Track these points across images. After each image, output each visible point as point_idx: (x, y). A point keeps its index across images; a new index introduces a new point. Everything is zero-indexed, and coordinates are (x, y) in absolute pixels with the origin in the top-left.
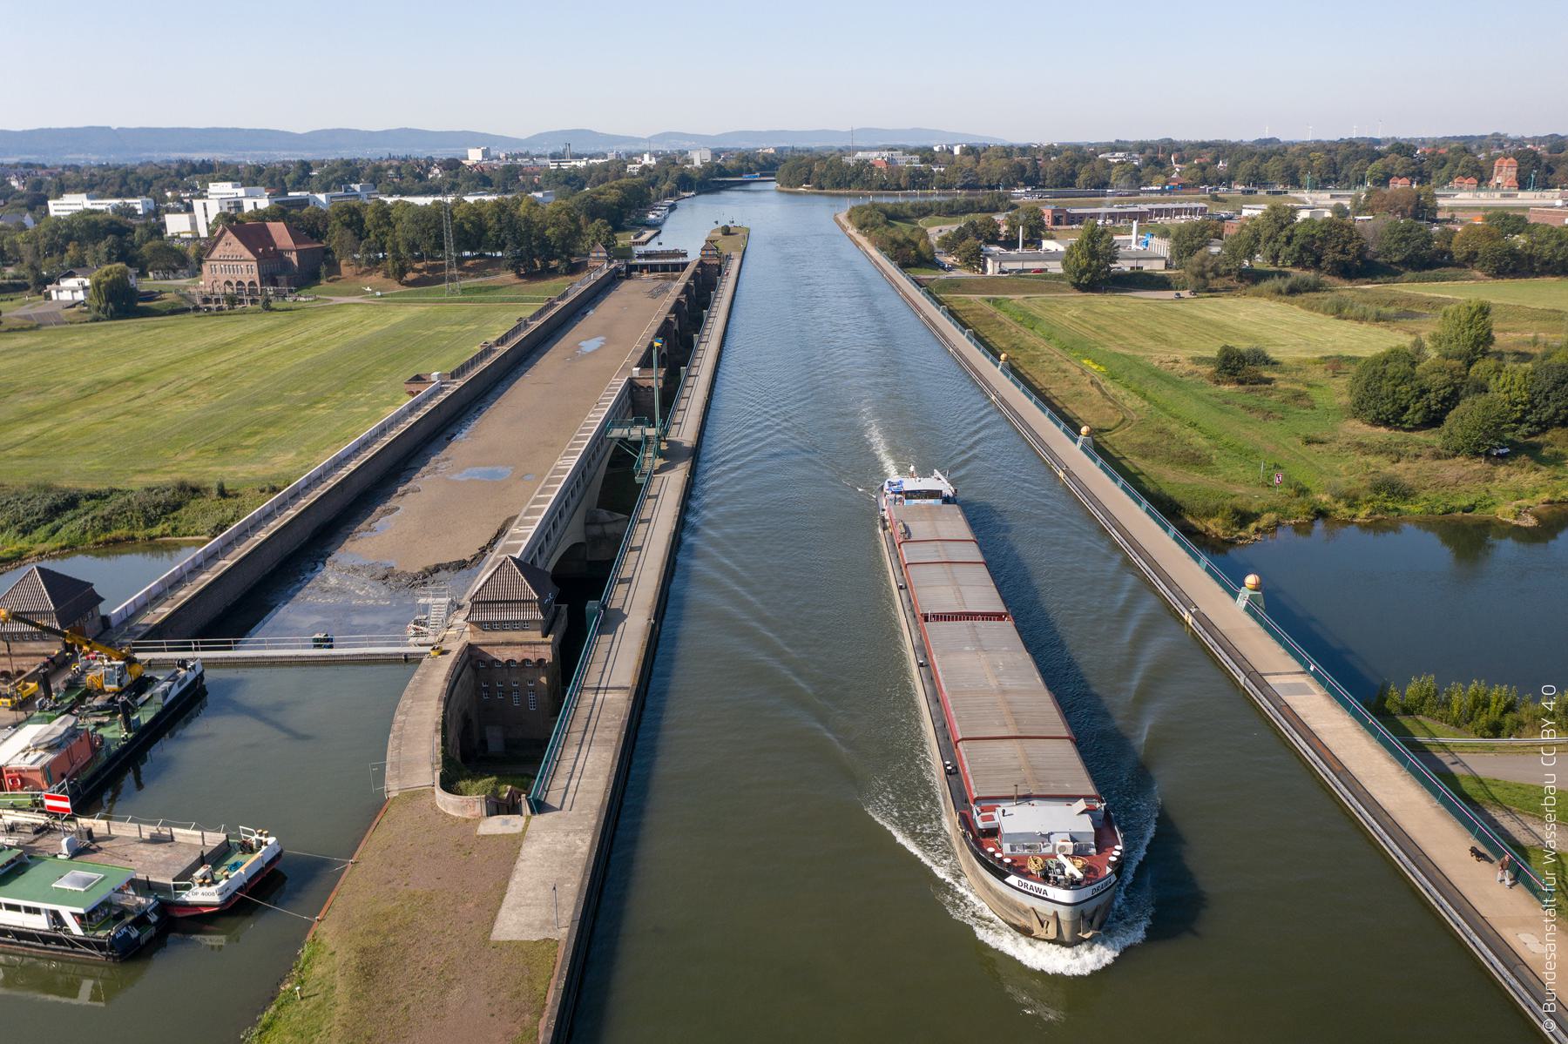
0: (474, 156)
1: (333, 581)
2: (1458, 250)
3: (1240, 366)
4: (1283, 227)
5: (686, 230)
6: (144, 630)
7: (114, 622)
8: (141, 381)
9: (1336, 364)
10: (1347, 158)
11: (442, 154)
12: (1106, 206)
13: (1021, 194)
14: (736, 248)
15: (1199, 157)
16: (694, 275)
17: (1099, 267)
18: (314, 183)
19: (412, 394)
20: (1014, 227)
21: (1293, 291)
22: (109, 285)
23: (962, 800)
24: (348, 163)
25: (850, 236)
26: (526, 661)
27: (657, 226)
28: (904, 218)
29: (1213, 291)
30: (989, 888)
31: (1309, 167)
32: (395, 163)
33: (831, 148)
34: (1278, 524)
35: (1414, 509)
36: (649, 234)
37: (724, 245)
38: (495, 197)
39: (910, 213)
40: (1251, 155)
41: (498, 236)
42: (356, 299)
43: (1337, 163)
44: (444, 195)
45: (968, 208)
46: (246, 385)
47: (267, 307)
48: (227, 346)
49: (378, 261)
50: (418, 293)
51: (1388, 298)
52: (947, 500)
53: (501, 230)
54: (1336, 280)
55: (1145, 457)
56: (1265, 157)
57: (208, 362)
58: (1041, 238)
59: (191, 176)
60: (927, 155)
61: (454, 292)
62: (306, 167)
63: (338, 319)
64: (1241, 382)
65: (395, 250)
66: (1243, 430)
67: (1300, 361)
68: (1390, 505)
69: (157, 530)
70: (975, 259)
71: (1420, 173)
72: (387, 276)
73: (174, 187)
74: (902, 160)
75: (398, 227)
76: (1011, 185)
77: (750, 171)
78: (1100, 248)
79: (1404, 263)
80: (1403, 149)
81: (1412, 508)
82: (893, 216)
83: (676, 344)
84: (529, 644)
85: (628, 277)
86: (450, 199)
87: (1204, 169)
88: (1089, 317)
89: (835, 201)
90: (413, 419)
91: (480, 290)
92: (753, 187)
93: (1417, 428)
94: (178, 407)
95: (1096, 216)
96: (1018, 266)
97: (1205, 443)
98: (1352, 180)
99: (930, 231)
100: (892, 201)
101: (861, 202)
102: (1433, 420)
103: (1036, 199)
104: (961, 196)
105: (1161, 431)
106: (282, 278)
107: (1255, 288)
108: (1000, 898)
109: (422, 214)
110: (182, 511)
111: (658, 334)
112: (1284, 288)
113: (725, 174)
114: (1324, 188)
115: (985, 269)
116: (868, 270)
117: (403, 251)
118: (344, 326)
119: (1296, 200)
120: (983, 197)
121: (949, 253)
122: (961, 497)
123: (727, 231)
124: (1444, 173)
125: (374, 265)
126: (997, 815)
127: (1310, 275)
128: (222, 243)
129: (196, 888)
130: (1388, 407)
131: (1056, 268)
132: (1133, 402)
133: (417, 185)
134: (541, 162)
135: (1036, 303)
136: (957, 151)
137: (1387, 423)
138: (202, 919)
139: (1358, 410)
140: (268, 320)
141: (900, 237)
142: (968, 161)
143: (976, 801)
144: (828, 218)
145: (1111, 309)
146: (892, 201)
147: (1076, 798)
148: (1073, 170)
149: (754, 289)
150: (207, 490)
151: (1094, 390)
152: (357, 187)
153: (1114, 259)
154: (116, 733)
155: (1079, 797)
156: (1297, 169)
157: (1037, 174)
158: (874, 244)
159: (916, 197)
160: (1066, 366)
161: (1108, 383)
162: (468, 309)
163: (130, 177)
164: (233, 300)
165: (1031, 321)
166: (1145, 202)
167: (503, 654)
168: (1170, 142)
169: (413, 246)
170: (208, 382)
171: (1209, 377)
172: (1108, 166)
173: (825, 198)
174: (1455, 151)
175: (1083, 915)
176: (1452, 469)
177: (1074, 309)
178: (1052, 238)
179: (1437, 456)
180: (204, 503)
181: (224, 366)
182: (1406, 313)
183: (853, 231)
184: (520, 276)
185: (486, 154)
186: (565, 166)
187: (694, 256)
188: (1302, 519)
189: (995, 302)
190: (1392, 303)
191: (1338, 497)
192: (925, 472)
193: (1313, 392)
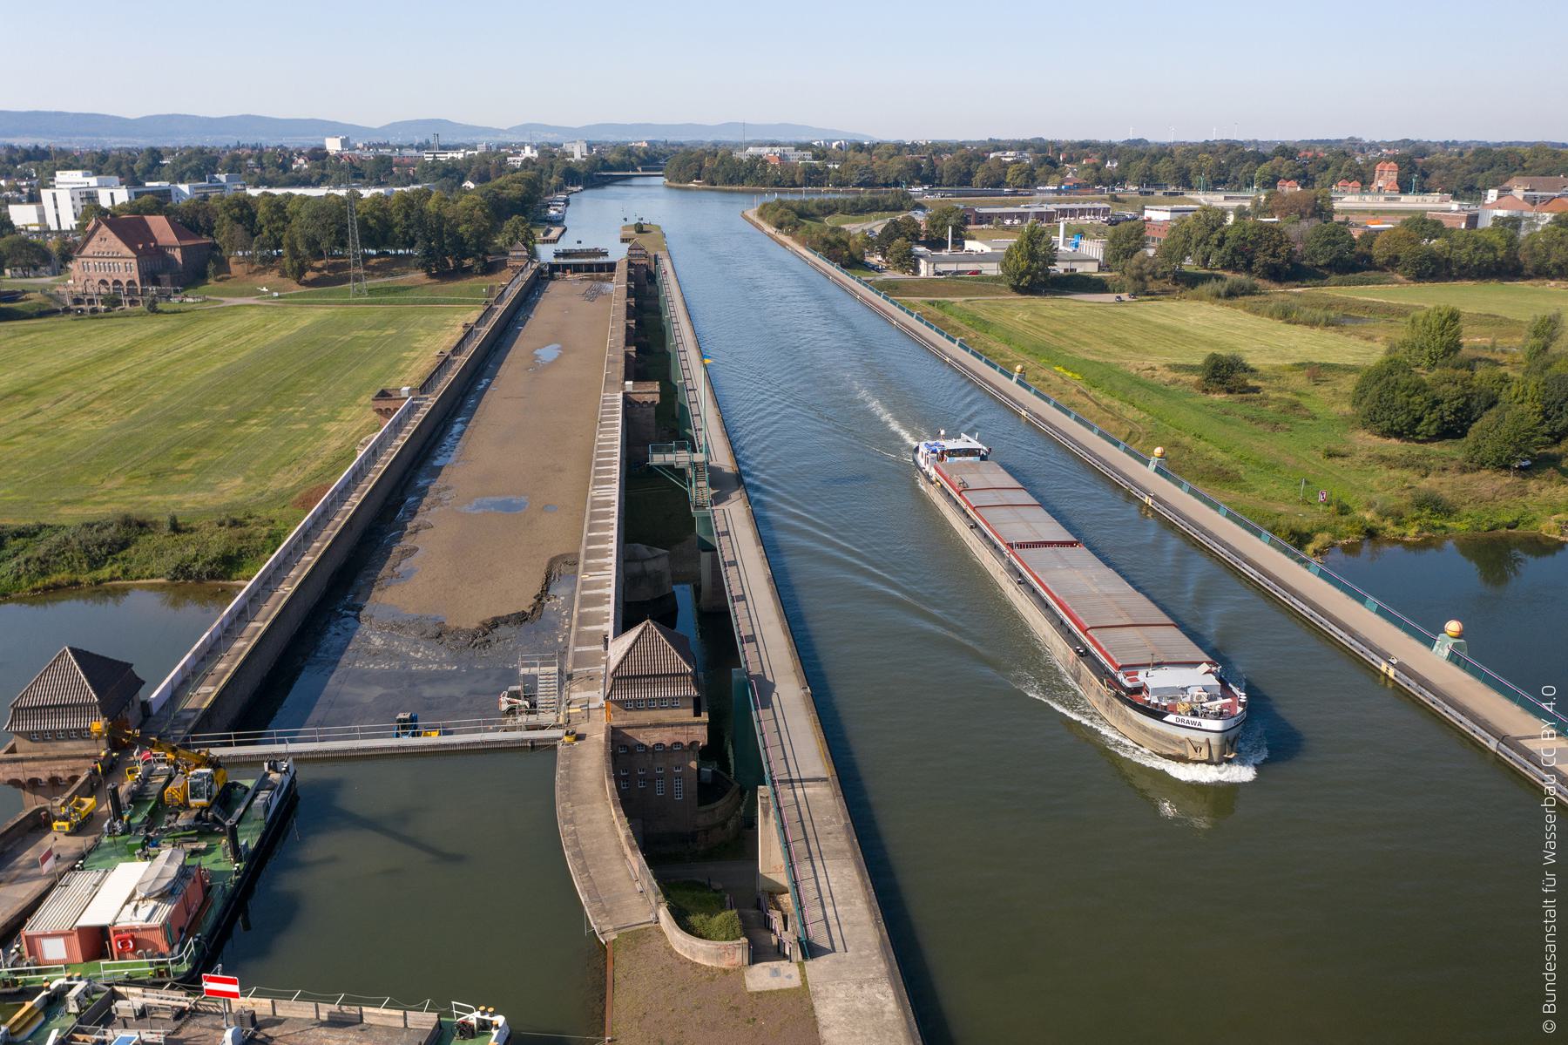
1: (377, 642)
2: (1378, 252)
3: (1224, 373)
4: (1214, 229)
6: (194, 719)
7: (155, 709)
11: (308, 142)
15: (1087, 157)
18: (167, 172)
21: (1231, 294)
24: (201, 151)
25: (769, 235)
27: (558, 222)
35: (1460, 526)
36: (555, 232)
38: (374, 191)
39: (815, 211)
41: (406, 233)
43: (1229, 164)
44: (337, 186)
46: (158, 398)
47: (153, 309)
49: (273, 259)
50: (320, 294)
54: (1267, 283)
57: (105, 371)
60: (822, 154)
61: (359, 293)
62: (155, 154)
63: (238, 323)
64: (1230, 391)
66: (1255, 443)
67: (1274, 368)
68: (1437, 523)
69: (105, 572)
70: (909, 262)
71: (1305, 175)
72: (283, 274)
74: (794, 157)
79: (1328, 266)
81: (1458, 525)
82: (803, 214)
83: (648, 350)
84: (682, 725)
85: (552, 278)
86: (342, 192)
88: (1040, 321)
89: (727, 198)
90: (400, 443)
91: (388, 291)
92: (636, 181)
93: (1431, 439)
96: (953, 267)
98: (1242, 180)
100: (797, 198)
102: (1452, 430)
104: (866, 194)
106: (166, 277)
107: (1191, 292)
109: (321, 209)
110: (132, 550)
111: (628, 344)
112: (1223, 291)
113: (608, 168)
115: (917, 270)
117: (302, 249)
118: (247, 331)
124: (1328, 175)
125: (268, 263)
127: (1242, 278)
128: (95, 239)
131: (992, 269)
134: (407, 152)
135: (981, 305)
137: (1399, 435)
139: (1370, 421)
140: (156, 325)
146: (797, 198)
150: (155, 524)
153: (1053, 261)
154: (221, 862)
156: (1188, 171)
157: (933, 172)
159: (828, 194)
160: (1044, 374)
162: (379, 312)
164: (112, 301)
165: (986, 326)
167: (650, 738)
169: (312, 243)
170: (111, 395)
171: (1197, 385)
173: (713, 194)
174: (1336, 155)
177: (1021, 312)
179: (1463, 470)
180: (158, 539)
181: (124, 377)
182: (1338, 319)
183: (771, 230)
184: (432, 276)
185: (344, 143)
186: (442, 157)
187: (618, 253)
188: (1353, 538)
189: (941, 306)
191: (1384, 514)
193: (1304, 401)
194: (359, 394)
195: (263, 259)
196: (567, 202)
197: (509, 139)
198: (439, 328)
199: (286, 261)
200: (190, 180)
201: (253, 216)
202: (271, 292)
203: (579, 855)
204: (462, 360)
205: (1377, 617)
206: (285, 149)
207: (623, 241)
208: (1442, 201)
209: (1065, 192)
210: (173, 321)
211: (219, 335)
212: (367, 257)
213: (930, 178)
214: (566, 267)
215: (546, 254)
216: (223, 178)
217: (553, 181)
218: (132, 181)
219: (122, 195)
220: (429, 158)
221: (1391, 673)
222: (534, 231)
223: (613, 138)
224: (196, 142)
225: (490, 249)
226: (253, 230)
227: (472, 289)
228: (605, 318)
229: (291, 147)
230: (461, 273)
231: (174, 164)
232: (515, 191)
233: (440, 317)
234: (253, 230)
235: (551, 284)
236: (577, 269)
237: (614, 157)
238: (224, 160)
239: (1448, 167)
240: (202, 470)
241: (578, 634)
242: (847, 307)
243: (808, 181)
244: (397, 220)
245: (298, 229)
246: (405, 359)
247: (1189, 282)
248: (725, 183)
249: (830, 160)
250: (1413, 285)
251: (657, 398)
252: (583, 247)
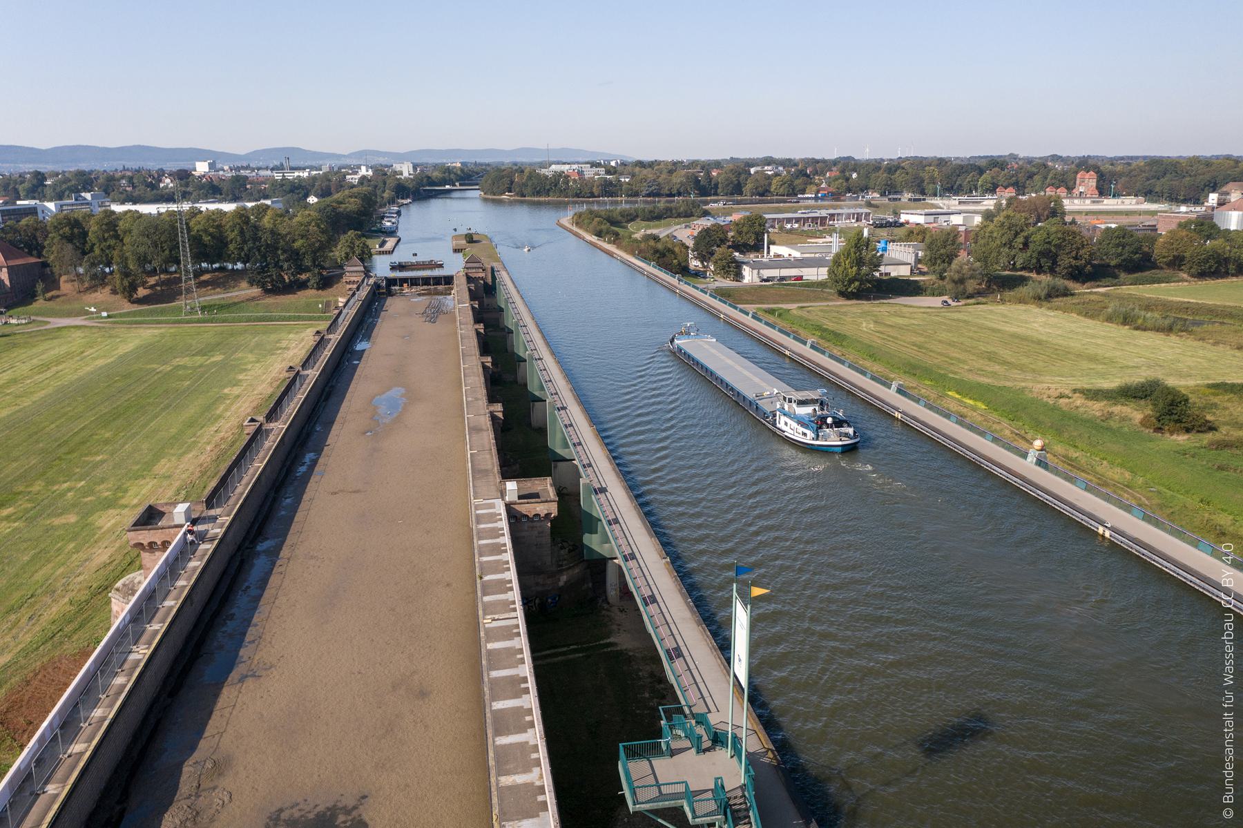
0: (202, 168)
2: (1158, 251)
32: (129, 174)
50: (151, 313)
65: (124, 260)
72: (114, 292)
74: (589, 172)
75: (127, 240)
79: (1118, 266)
85: (390, 294)
91: (222, 307)
104: (662, 203)
107: (1009, 294)
109: (153, 226)
113: (430, 185)
115: (739, 276)
125: (99, 281)
133: (150, 193)
134: (262, 173)
152: (88, 196)
156: (923, 181)
162: (210, 331)
169: (143, 260)
171: (1144, 423)
177: (863, 319)
183: (594, 239)
185: (211, 166)
186: (291, 176)
196: (399, 213)
197: (348, 162)
198: (275, 350)
201: (85, 234)
202: (99, 312)
204: (313, 374)
207: (456, 251)
208: (1137, 203)
209: (822, 199)
214: (403, 281)
215: (382, 267)
217: (386, 195)
220: (278, 176)
221: (1107, 534)
222: (369, 242)
223: (432, 160)
225: (327, 265)
227: (308, 305)
232: (352, 205)
233: (273, 337)
235: (389, 300)
237: (436, 175)
239: (1129, 174)
241: (484, 586)
244: (232, 236)
245: (131, 246)
246: (226, 397)
252: (420, 259)
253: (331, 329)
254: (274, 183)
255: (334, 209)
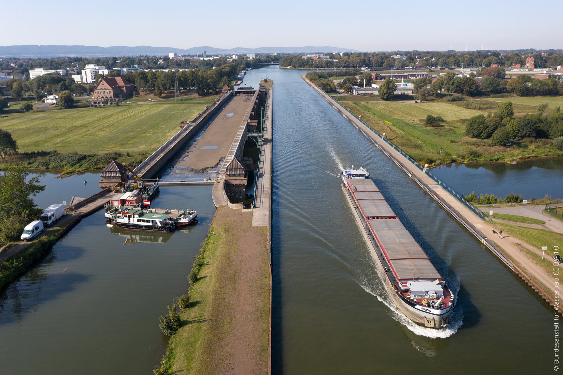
2: (509, 88)
3: (433, 122)
4: (451, 80)
5: (252, 80)
8: (86, 126)
9: (463, 121)
10: (476, 57)
11: (163, 55)
12: (391, 74)
13: (364, 69)
14: (270, 86)
16: (258, 94)
17: (390, 93)
19: (182, 127)
20: (362, 80)
21: (454, 100)
22: (65, 97)
23: (393, 281)
24: (129, 58)
25: (307, 83)
26: (240, 184)
27: (241, 79)
28: (325, 77)
29: (427, 101)
30: (407, 310)
31: (463, 60)
33: (296, 53)
34: (441, 164)
36: (239, 82)
37: (266, 85)
40: (444, 56)
42: (146, 103)
43: (472, 59)
45: (346, 74)
46: (121, 127)
47: (117, 105)
48: (109, 116)
49: (152, 90)
50: (166, 101)
51: (485, 103)
52: (367, 178)
53: (193, 80)
54: (468, 97)
55: (403, 146)
56: (448, 57)
57: (106, 121)
58: (371, 83)
59: (79, 63)
60: (331, 56)
61: (178, 100)
62: (115, 59)
63: (142, 109)
64: (433, 126)
67: (453, 121)
68: (474, 158)
71: (501, 62)
72: (155, 95)
73: (69, 66)
74: (323, 57)
76: (360, 66)
77: (270, 62)
78: (391, 86)
80: (496, 54)
81: (482, 160)
82: (321, 76)
83: (258, 113)
85: (236, 95)
87: (427, 61)
89: (300, 71)
90: (186, 133)
91: (186, 100)
92: (270, 67)
93: (485, 138)
94: (101, 134)
95: (390, 76)
96: (364, 92)
97: (421, 142)
99: (334, 81)
100: (320, 71)
101: (310, 72)
102: (489, 136)
103: (369, 71)
104: (344, 70)
105: (408, 139)
108: (412, 313)
111: (252, 111)
112: (451, 99)
113: (261, 62)
114: (468, 67)
115: (353, 93)
116: (315, 93)
118: (145, 111)
119: (458, 71)
120: (351, 70)
121: (340, 88)
122: (371, 176)
123: (266, 81)
124: (509, 62)
125: (151, 91)
126: (408, 285)
127: (460, 95)
128: (101, 84)
129: (182, 219)
130: (476, 132)
131: (376, 93)
132: (400, 132)
135: (370, 104)
136: (341, 54)
137: (476, 137)
138: (184, 226)
139: (468, 133)
140: (119, 109)
141: (325, 83)
142: (346, 58)
143: (400, 280)
144: (298, 79)
145: (394, 106)
146: (320, 71)
147: (435, 279)
148: (382, 61)
149: (277, 99)
151: (388, 128)
153: (395, 90)
155: (436, 279)
156: (459, 61)
157: (370, 62)
158: (316, 85)
159: (328, 70)
160: (379, 122)
161: (392, 127)
162: (183, 106)
163: (54, 63)
165: (369, 109)
166: (407, 72)
167: (234, 183)
168: (417, 51)
169: (164, 85)
170: (108, 126)
171: (424, 125)
172: (394, 60)
175: (443, 318)
176: (493, 149)
177: (382, 106)
178: (375, 83)
179: (490, 145)
180: (124, 158)
182: (490, 107)
183: (308, 81)
184: (200, 95)
185: (175, 55)
186: (206, 59)
187: (257, 88)
188: (448, 162)
189: (356, 104)
190: (486, 104)
192: (357, 168)
193: (456, 130)
194: (176, 127)
195: (149, 90)
197: (230, 53)
199: (156, 91)
200: (126, 67)
201: (146, 77)
203: (215, 197)
205: (416, 167)
206: (156, 57)
209: (415, 69)
210: (123, 108)
211: (137, 112)
212: (180, 90)
213: (368, 64)
214: (240, 92)
215: (236, 88)
216: (136, 66)
217: (241, 67)
218: (108, 68)
219: (106, 72)
220: (202, 59)
221: (485, 243)
224: (127, 55)
225: (218, 87)
226: (146, 81)
228: (246, 106)
229: (158, 57)
230: (209, 94)
231: (121, 62)
232: (227, 69)
234: (146, 81)
236: (244, 93)
237: (263, 58)
238: (137, 61)
240: (134, 144)
242: (323, 102)
243: (327, 66)
244: (190, 78)
245: (160, 81)
247: (441, 96)
248: (299, 67)
249: (335, 59)
250: (519, 98)
251: (256, 124)
253: (211, 106)
254: (200, 62)
255: (221, 71)
